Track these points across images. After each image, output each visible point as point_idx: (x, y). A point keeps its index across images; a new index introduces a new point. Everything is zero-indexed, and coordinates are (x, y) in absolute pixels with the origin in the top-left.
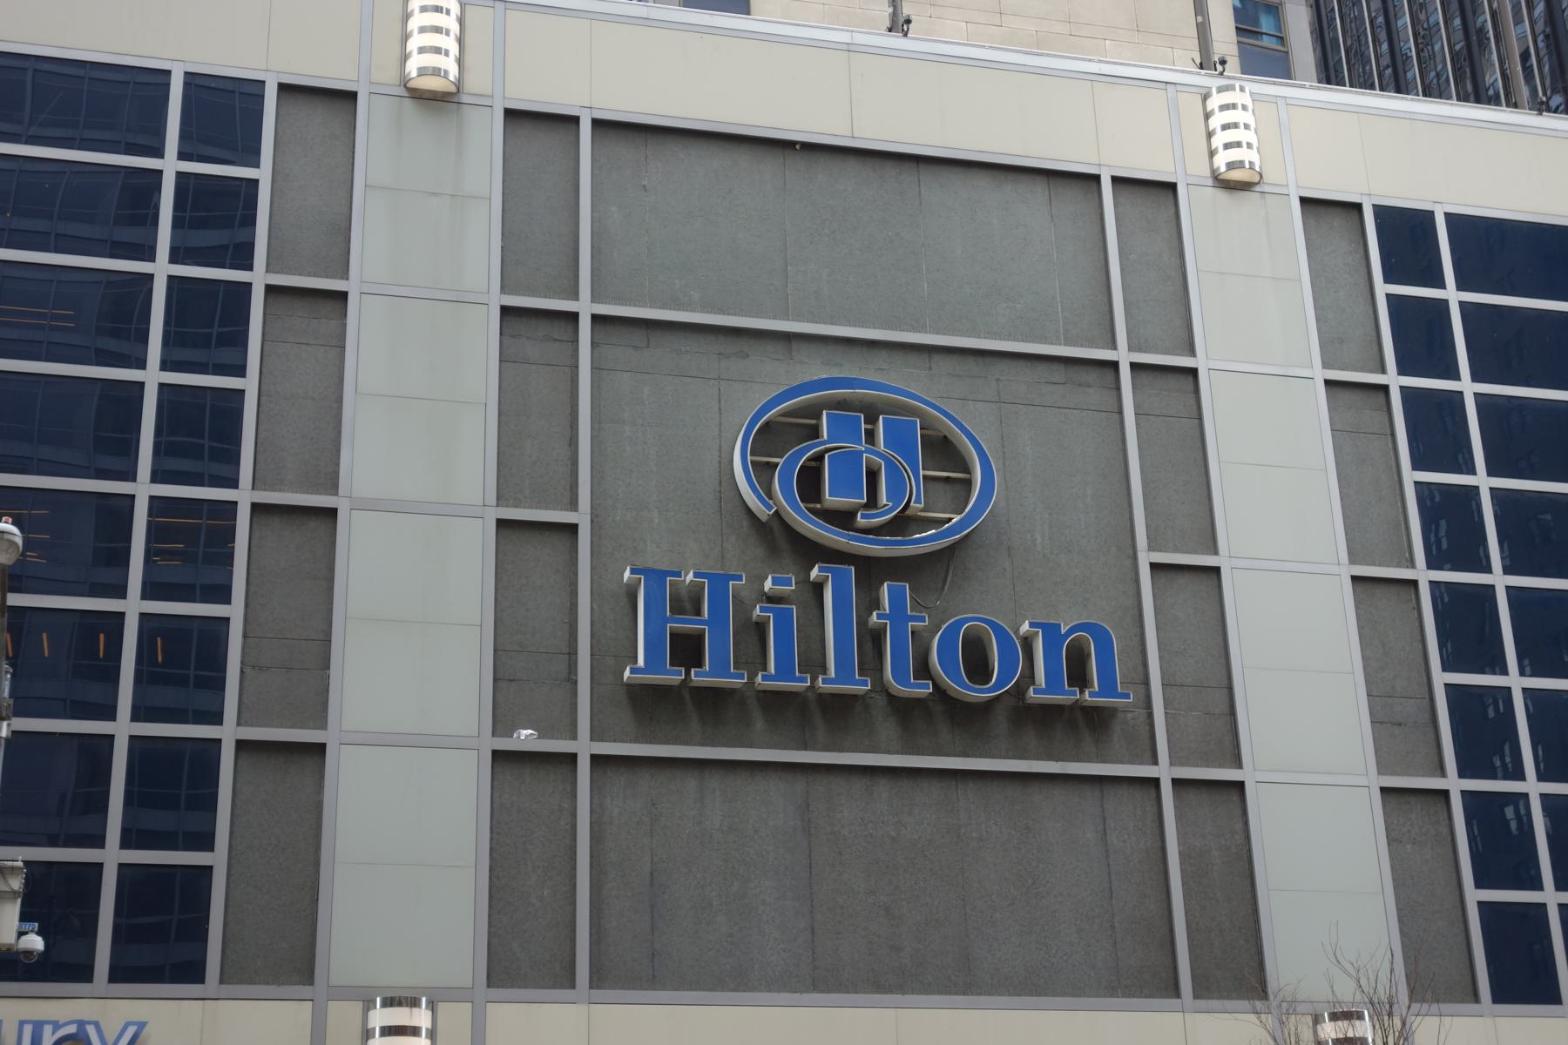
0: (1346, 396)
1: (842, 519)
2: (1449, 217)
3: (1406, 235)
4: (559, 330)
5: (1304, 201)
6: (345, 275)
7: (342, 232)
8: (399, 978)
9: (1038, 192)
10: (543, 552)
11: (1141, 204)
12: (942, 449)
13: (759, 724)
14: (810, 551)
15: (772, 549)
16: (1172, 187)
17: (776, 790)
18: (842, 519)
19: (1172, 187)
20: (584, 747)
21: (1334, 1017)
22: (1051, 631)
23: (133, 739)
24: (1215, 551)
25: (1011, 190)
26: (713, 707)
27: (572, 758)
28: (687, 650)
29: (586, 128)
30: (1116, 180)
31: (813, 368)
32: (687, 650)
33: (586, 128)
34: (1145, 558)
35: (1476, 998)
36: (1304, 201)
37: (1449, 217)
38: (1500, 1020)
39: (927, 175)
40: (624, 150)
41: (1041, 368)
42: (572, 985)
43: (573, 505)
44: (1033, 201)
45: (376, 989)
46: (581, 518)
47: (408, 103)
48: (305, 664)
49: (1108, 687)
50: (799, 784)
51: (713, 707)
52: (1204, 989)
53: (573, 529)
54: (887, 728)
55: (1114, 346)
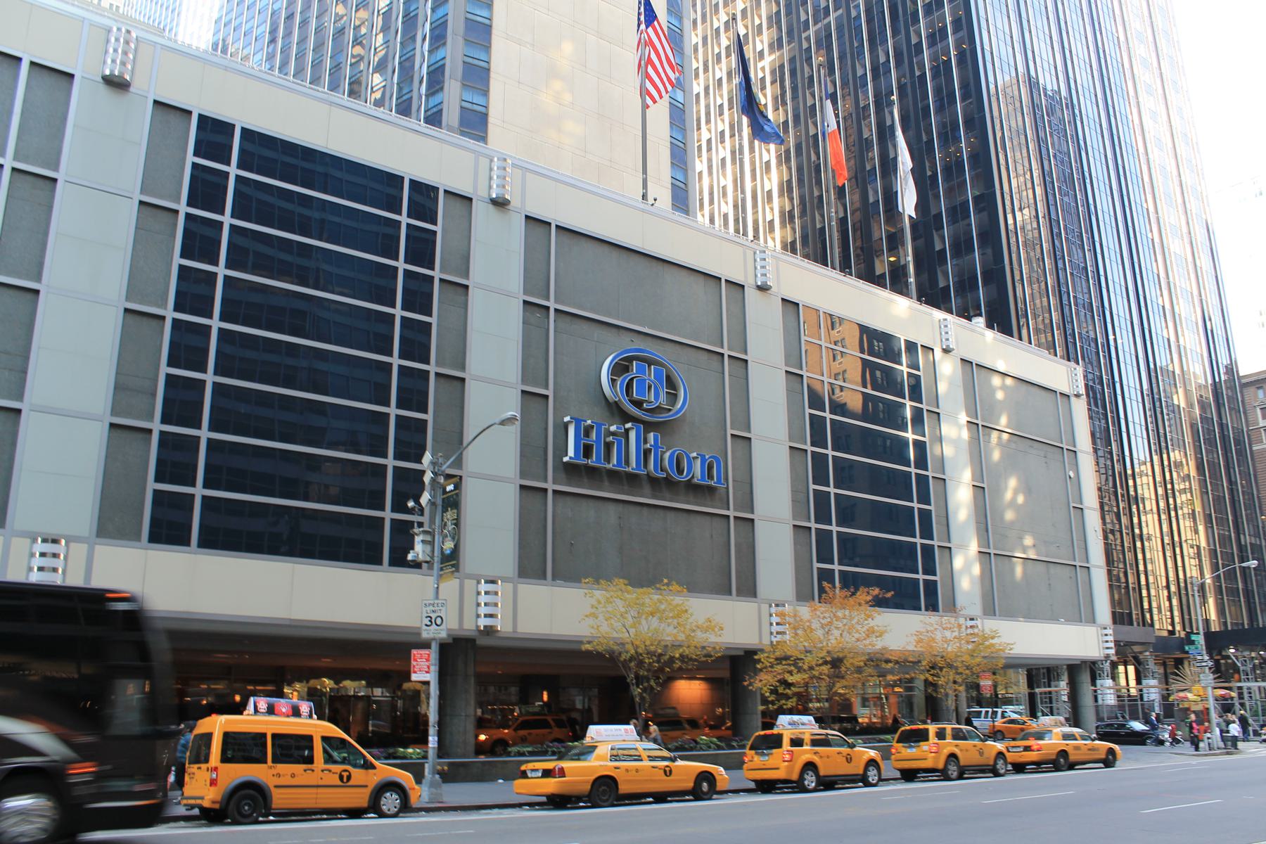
0: (790, 377)
1: (638, 404)
2: (243, 129)
3: (214, 134)
4: (166, 216)
5: (155, 102)
6: (56, 169)
7: (466, 259)
8: (491, 574)
9: (701, 279)
10: (535, 404)
11: (458, 205)
12: (671, 383)
13: (606, 483)
14: (626, 417)
15: (612, 414)
16: (471, 199)
17: (612, 510)
18: (638, 404)
19: (471, 199)
20: (550, 486)
21: (486, 582)
22: (703, 457)
23: (386, 466)
24: (749, 432)
25: (692, 278)
26: (592, 474)
27: (150, 431)
28: (587, 451)
29: (25, 67)
30: (446, 191)
31: (639, 344)
32: (587, 451)
33: (25, 67)
34: (730, 432)
35: (730, 594)
36: (155, 102)
37: (243, 129)
38: (150, 552)
39: (666, 266)
40: (566, 238)
41: (159, 212)
42: (544, 577)
43: (547, 387)
44: (699, 285)
45: (39, 534)
46: (550, 393)
47: (491, 206)
48: (454, 442)
49: (719, 481)
50: (620, 507)
51: (592, 474)
52: (739, 593)
53: (546, 397)
54: (647, 489)
55: (722, 347)
